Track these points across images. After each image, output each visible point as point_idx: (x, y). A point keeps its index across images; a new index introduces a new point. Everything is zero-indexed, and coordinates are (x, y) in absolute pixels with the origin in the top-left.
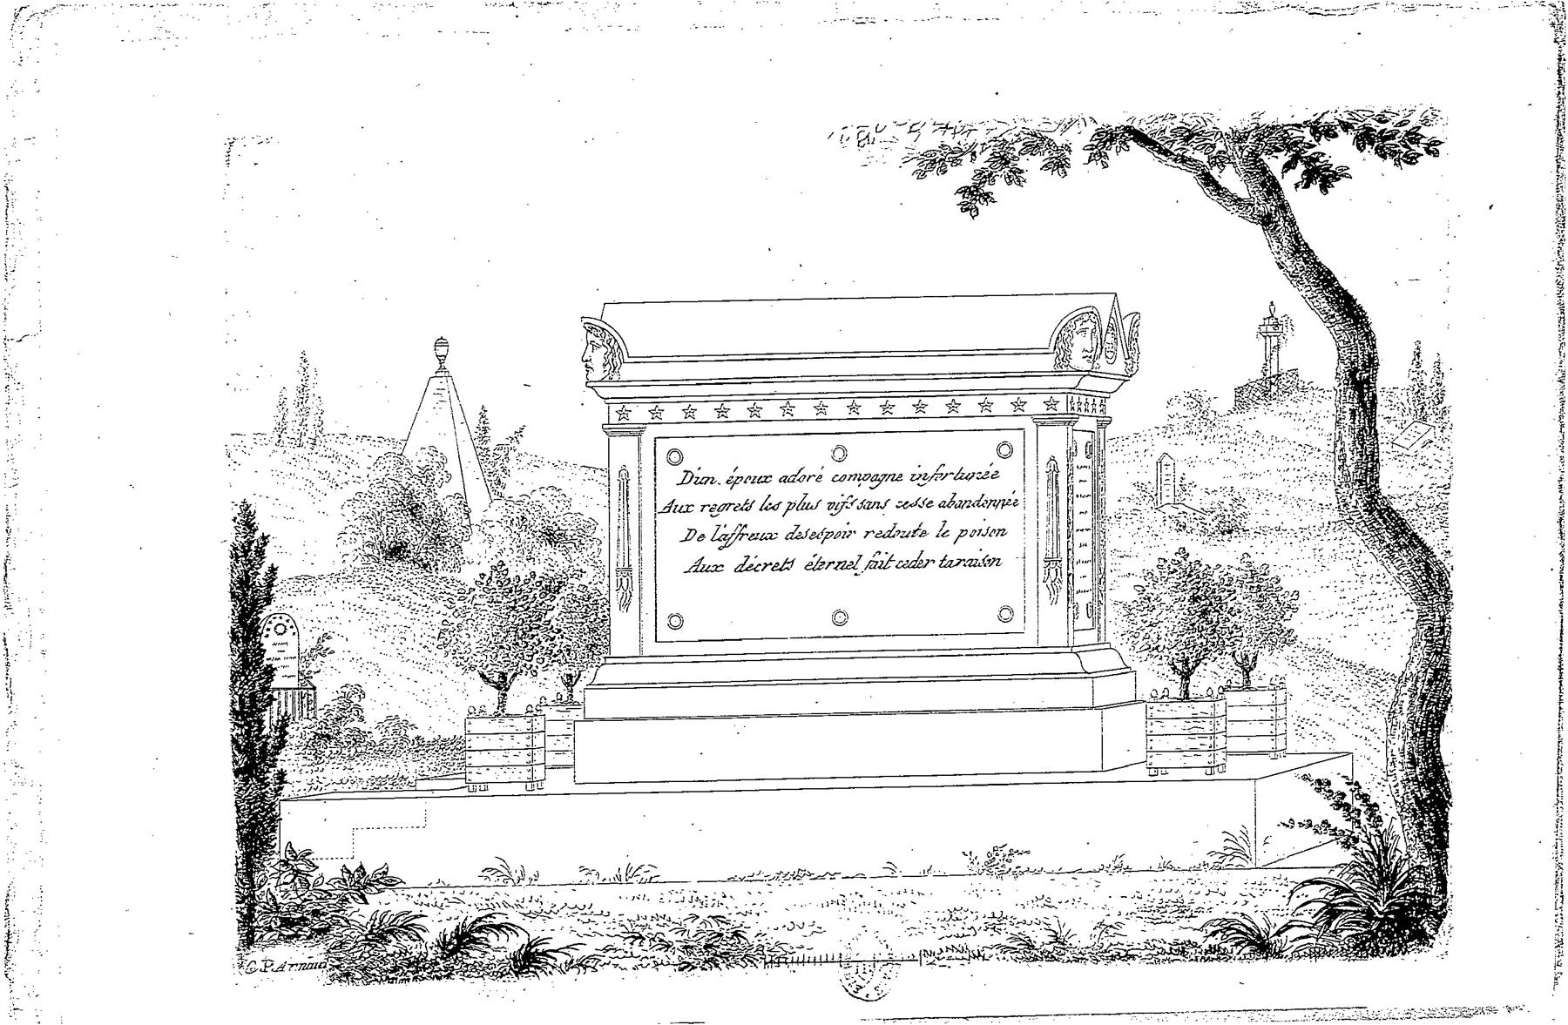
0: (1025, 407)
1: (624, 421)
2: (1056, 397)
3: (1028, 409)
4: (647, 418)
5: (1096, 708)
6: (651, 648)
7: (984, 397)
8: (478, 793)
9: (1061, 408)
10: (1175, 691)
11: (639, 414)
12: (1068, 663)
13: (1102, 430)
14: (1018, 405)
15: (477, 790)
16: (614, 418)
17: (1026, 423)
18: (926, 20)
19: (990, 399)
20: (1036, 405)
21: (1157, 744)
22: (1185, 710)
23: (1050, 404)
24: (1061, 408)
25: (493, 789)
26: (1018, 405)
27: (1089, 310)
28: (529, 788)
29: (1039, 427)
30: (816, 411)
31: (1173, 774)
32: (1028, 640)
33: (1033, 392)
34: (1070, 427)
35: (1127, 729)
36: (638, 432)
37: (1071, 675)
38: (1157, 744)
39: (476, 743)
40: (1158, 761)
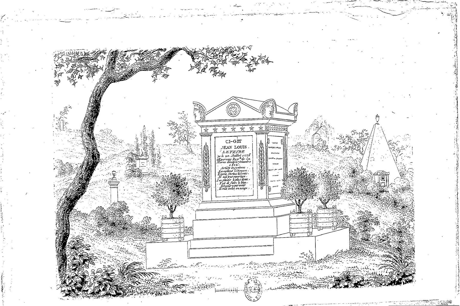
0: (262, 129)
1: (261, 130)
2: (262, 126)
3: (254, 130)
4: (213, 131)
5: (275, 217)
6: (214, 199)
7: (215, 127)
8: (165, 241)
9: (264, 129)
10: (168, 217)
11: (211, 130)
12: (266, 204)
13: (286, 136)
14: (251, 128)
15: (165, 240)
16: (203, 131)
17: (253, 134)
18: (40, 20)
19: (225, 127)
20: (256, 128)
21: (293, 226)
22: (171, 221)
23: (261, 128)
24: (264, 129)
25: (297, 235)
26: (251, 128)
27: (272, 100)
28: (291, 235)
29: (203, 137)
30: (232, 130)
31: (297, 235)
32: (255, 197)
33: (219, 126)
34: (266, 135)
35: (284, 223)
36: (210, 135)
37: (268, 207)
38: (293, 226)
39: (164, 226)
40: (293, 231)
